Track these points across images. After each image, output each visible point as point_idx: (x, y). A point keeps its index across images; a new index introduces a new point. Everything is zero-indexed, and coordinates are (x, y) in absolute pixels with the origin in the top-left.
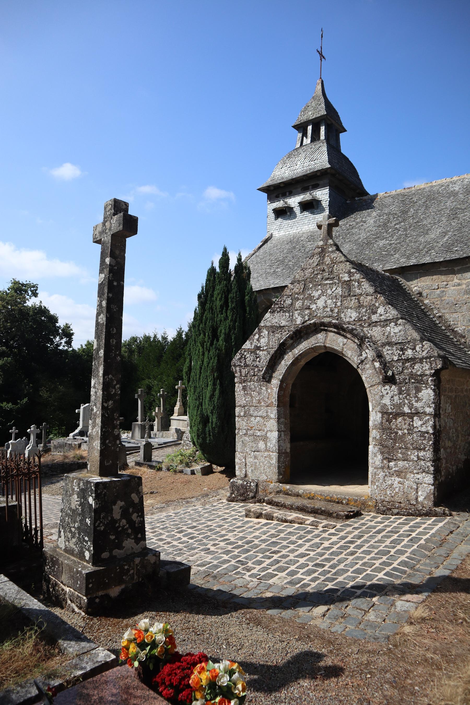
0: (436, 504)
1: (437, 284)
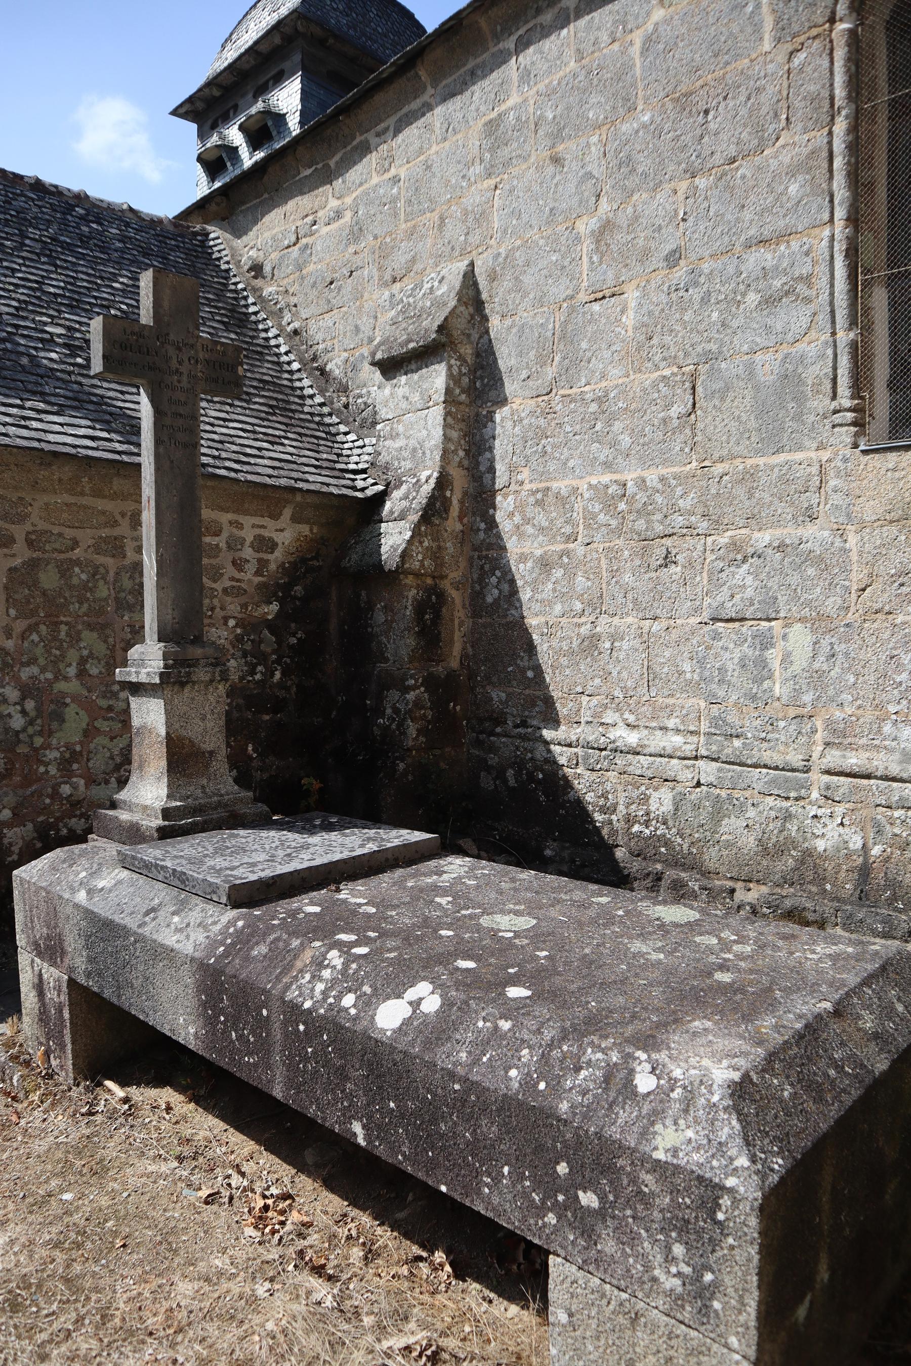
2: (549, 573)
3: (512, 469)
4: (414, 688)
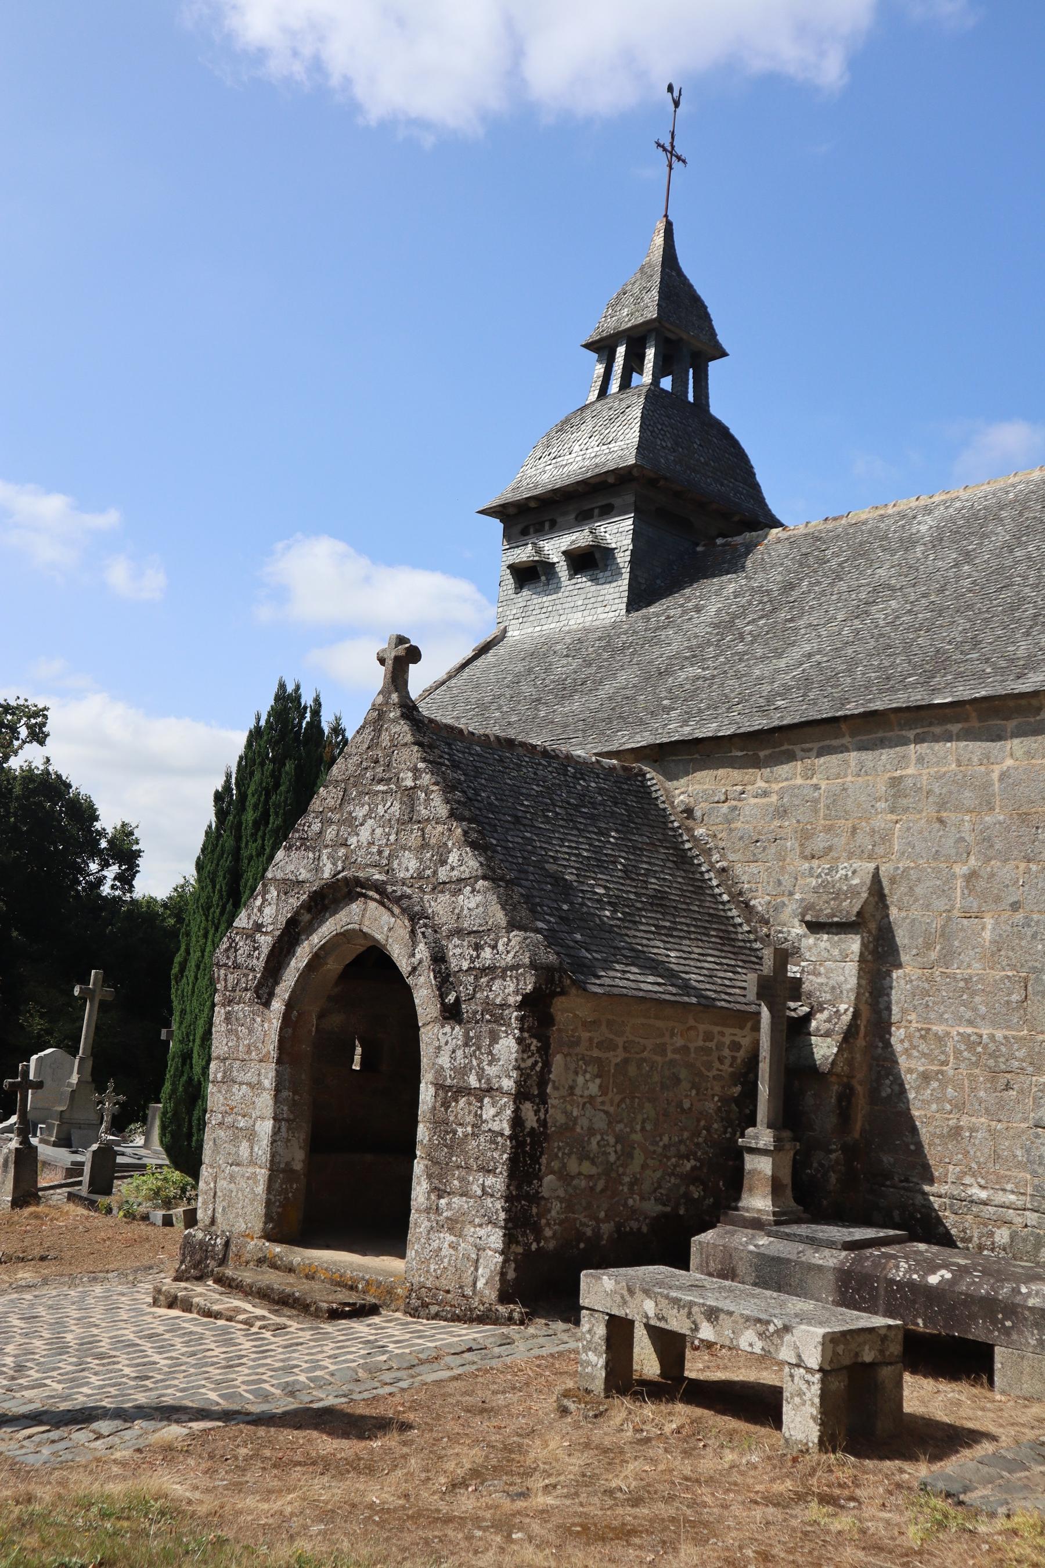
0: (504, 1298)
1: (724, 790)
2: (928, 1083)
3: (904, 1011)
4: (835, 1151)
